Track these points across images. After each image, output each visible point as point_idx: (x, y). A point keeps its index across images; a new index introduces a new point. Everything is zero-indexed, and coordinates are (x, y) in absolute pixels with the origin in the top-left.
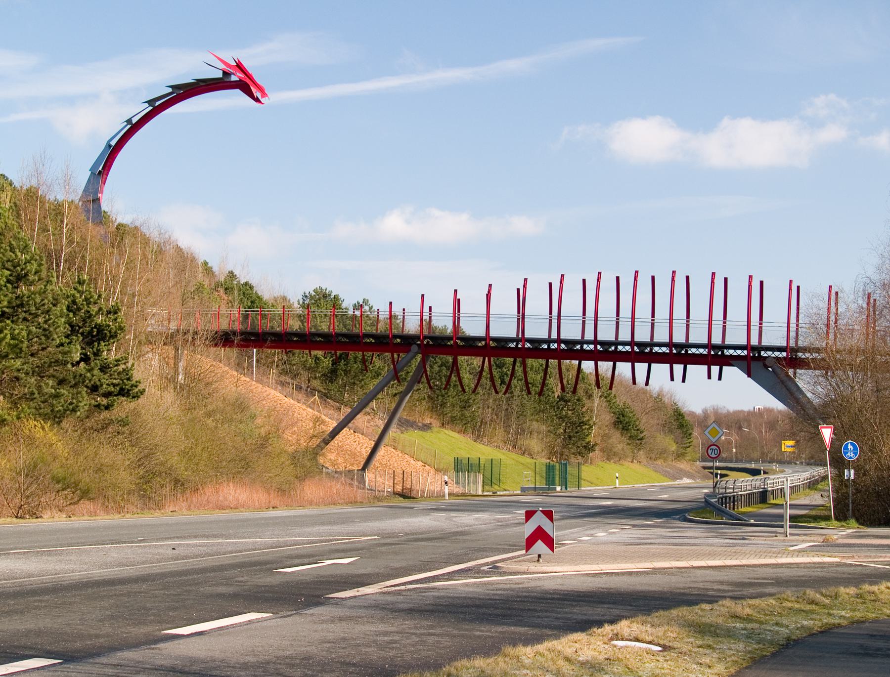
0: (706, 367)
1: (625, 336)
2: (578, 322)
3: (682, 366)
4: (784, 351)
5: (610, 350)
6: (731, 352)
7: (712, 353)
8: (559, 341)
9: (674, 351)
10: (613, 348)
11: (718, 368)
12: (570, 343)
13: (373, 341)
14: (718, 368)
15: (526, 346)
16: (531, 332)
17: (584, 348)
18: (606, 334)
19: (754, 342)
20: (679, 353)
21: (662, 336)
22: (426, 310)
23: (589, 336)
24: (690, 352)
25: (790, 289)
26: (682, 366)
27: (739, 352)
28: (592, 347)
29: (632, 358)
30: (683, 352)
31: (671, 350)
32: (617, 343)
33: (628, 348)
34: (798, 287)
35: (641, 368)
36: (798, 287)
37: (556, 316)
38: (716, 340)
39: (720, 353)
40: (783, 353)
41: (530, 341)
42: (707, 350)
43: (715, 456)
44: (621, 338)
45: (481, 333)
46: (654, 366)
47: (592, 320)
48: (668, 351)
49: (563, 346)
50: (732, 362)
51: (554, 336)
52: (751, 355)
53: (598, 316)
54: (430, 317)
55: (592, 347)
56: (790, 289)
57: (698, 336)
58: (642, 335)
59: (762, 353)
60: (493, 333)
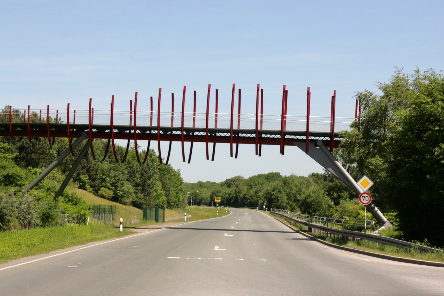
0: (205, 143)
1: (177, 125)
2: (197, 116)
3: (190, 143)
4: (254, 133)
5: (168, 133)
6: (221, 134)
7: (209, 134)
8: (135, 128)
9: (209, 134)
10: (170, 133)
11: (212, 144)
12: (165, 130)
13: (20, 129)
14: (212, 144)
15: (137, 132)
16: (139, 123)
17: (152, 132)
18: (165, 123)
19: (235, 127)
20: (188, 135)
21: (201, 124)
22: (71, 112)
23: (155, 124)
24: (195, 134)
25: (233, 90)
26: (190, 143)
27: (249, 135)
28: (156, 132)
29: (159, 138)
30: (191, 134)
31: (182, 133)
32: (172, 129)
33: (179, 133)
34: (240, 90)
35: (165, 144)
36: (240, 90)
37: (156, 114)
38: (211, 126)
39: (214, 135)
40: (155, 131)
41: (140, 128)
42: (205, 133)
43: (367, 202)
44: (197, 126)
45: (107, 122)
46: (173, 143)
47: (219, 116)
48: (181, 134)
49: (138, 131)
50: (294, 143)
51: (133, 124)
52: (233, 136)
53: (137, 111)
54: (41, 114)
55: (156, 132)
56: (233, 90)
57: (224, 124)
58: (188, 124)
59: (240, 135)
60: (115, 123)
